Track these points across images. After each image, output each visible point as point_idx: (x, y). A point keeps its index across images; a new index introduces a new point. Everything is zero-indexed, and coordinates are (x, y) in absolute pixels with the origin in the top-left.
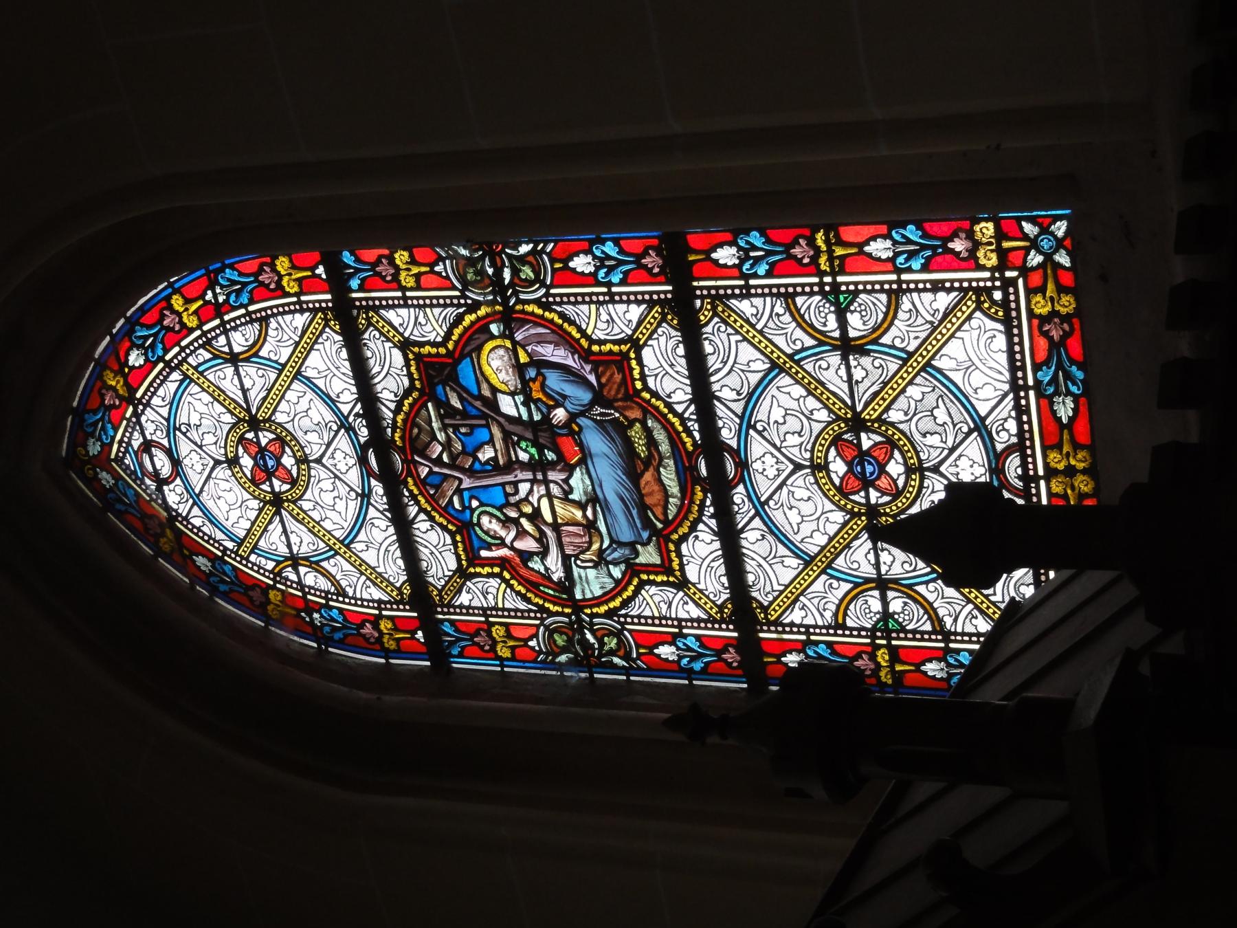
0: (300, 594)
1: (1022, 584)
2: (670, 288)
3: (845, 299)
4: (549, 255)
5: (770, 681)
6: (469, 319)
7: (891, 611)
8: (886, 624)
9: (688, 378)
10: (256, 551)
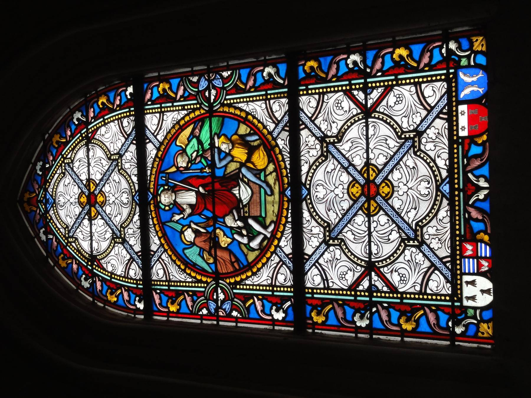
1: (429, 226)
2: (286, 90)
3: (302, 114)
4: (227, 91)
5: (154, 313)
6: (244, 277)
7: (280, 245)
8: (218, 314)
9: (304, 232)
10: (433, 268)
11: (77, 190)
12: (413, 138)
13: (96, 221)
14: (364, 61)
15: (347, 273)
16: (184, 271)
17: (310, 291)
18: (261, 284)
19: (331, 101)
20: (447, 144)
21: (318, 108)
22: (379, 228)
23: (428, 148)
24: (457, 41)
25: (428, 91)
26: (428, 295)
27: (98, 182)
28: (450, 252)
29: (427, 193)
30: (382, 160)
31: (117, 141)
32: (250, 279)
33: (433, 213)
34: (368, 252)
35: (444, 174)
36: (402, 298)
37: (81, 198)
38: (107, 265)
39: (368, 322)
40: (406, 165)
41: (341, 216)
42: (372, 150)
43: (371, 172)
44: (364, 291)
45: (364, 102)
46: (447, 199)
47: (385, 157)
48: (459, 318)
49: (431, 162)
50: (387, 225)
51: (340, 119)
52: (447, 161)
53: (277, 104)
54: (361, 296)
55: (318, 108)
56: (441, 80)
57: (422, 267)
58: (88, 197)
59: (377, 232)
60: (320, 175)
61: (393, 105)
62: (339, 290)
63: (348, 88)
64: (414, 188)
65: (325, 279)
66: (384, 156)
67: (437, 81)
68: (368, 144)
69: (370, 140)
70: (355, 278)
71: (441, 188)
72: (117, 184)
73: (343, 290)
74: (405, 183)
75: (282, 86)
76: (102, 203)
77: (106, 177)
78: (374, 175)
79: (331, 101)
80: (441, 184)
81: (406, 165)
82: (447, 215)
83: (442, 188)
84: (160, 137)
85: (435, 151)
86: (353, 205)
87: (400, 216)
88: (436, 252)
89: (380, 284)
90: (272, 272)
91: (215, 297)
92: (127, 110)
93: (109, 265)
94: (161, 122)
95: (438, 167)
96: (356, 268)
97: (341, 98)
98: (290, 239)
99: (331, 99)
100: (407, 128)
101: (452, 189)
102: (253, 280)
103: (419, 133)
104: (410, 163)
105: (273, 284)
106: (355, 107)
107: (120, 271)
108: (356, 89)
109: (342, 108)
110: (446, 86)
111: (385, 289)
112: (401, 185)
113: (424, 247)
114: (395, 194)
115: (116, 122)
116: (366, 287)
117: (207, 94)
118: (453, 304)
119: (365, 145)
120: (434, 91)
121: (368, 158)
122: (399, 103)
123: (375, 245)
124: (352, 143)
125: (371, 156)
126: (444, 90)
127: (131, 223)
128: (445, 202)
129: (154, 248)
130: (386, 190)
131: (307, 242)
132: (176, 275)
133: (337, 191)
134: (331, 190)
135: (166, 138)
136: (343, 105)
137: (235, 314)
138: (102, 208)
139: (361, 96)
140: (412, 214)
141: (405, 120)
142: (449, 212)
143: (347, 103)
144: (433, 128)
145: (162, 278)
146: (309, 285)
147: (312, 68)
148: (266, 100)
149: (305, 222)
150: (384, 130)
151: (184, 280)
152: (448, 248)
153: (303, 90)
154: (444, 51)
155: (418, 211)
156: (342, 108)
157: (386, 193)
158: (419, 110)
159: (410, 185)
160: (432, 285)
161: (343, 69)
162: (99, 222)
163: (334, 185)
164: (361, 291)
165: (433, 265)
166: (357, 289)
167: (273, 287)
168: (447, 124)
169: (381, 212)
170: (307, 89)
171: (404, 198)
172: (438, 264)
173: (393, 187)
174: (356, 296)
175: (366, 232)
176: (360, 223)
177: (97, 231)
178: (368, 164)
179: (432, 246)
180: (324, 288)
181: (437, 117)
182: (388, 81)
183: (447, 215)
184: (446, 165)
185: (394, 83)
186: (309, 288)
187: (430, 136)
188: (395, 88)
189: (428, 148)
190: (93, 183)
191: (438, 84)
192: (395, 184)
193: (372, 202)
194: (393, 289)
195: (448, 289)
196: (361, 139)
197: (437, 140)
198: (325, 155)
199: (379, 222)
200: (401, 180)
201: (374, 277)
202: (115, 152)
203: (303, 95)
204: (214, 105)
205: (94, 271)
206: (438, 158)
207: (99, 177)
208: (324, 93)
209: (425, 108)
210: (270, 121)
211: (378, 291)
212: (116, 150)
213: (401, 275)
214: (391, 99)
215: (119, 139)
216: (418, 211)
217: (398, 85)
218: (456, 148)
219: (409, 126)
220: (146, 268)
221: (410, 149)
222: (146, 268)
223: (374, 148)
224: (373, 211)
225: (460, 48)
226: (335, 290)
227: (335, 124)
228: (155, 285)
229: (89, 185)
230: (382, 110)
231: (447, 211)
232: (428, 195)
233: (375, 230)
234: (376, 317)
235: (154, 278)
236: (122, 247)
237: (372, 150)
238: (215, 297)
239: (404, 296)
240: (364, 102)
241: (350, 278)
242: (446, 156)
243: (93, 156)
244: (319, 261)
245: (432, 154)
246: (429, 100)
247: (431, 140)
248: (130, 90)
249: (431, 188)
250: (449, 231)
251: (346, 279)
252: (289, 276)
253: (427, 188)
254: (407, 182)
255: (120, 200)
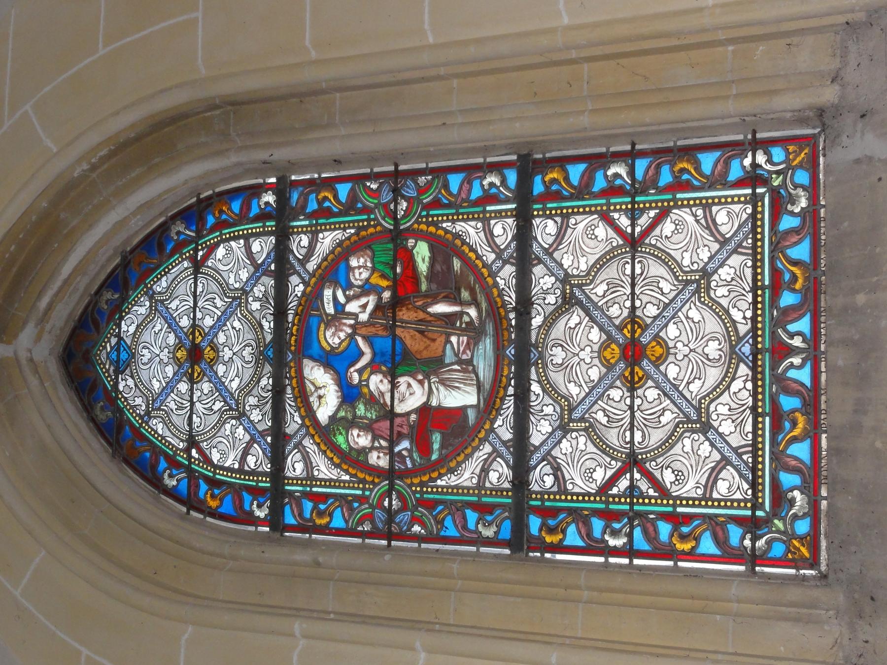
0: (187, 463)
11: (172, 339)
12: (571, 420)
13: (199, 385)
14: (632, 173)
15: (595, 470)
16: (337, 466)
17: (539, 496)
18: (684, 495)
19: (691, 484)
20: (514, 297)
21: (560, 236)
22: (646, 405)
23: (719, 293)
24: (767, 153)
25: (256, 247)
26: (713, 500)
27: (207, 330)
28: (270, 424)
29: (718, 357)
30: (652, 311)
31: (566, 253)
32: (445, 478)
33: (723, 386)
34: (628, 439)
35: (743, 329)
36: (674, 506)
37: (177, 351)
38: (662, 470)
39: (625, 540)
40: (687, 318)
41: (164, 385)
42: (638, 296)
43: (197, 334)
44: (620, 497)
45: (629, 230)
46: (114, 366)
47: (656, 307)
48: (760, 532)
49: (722, 314)
50: (656, 402)
51: (595, 251)
52: (272, 323)
53: (499, 226)
54: (614, 503)
55: (560, 236)
56: (739, 202)
57: (243, 441)
58: (190, 352)
59: (625, 294)
60: (558, 331)
61: (598, 468)
62: (583, 495)
63: (629, 206)
64: (699, 350)
65: (248, 248)
66: (654, 305)
67: (733, 202)
68: (633, 285)
69: (636, 280)
70: (607, 477)
71: (737, 350)
72: (697, 325)
73: (589, 494)
74: (686, 343)
75: (507, 201)
76: (658, 359)
77: (220, 323)
78: (200, 338)
79: (581, 226)
80: (737, 344)
81: (687, 318)
82: (745, 387)
83: (740, 350)
84: (311, 266)
85: (542, 403)
86: (606, 374)
87: (677, 389)
88: (726, 438)
89: (644, 485)
90: (706, 475)
91: (386, 503)
92: (365, 217)
93: (214, 451)
94: (485, 471)
95: (734, 322)
96: (610, 464)
97: (595, 222)
98: (291, 294)
99: (581, 224)
100: (689, 266)
101: (755, 352)
102: (449, 479)
103: (706, 274)
104: (694, 314)
105: (708, 496)
106: (615, 236)
107: (690, 488)
108: (615, 210)
109: (673, 472)
110: (274, 241)
111: (651, 492)
112: (679, 345)
113: (559, 433)
114: (671, 358)
115: (242, 241)
116: (622, 489)
117: (392, 206)
118: (754, 513)
119: (192, 302)
120: (262, 247)
121: (633, 308)
122: (678, 232)
123: (638, 429)
124: (660, 422)
125: (638, 303)
126: (745, 216)
127: (727, 392)
128: (744, 370)
129: (509, 270)
130: (659, 350)
131: (738, 273)
132: (324, 469)
133: (582, 355)
134: (695, 352)
135: (319, 267)
136: (672, 478)
137: (417, 528)
138: (657, 367)
139: (624, 222)
140: (695, 387)
141: (581, 446)
142: (271, 380)
143: (602, 231)
144: (726, 267)
145: (550, 488)
146: (535, 487)
147: (492, 185)
148: (486, 221)
149: (271, 318)
150: (656, 269)
151: (336, 478)
152: (747, 436)
153: (538, 210)
154: (747, 162)
155: (704, 382)
156: (596, 237)
157: (657, 355)
158: (563, 457)
159: (692, 346)
160: (722, 487)
161: (255, 211)
162: (206, 387)
163: (690, 360)
164: (614, 496)
165: (724, 458)
166: (610, 492)
167: (632, 496)
168: (273, 282)
169: (617, 322)
170: (544, 209)
171: (684, 364)
172: (734, 458)
173: (668, 348)
174: (607, 503)
175: (626, 412)
176: (617, 399)
177: (642, 408)
178: (194, 326)
179: (721, 430)
180: (559, 492)
181: (735, 251)
182: (663, 201)
183: (745, 387)
184: (745, 318)
185: (672, 204)
186: (537, 493)
187: (723, 278)
188: (674, 211)
189: (719, 293)
190: (199, 331)
191: (736, 208)
192: (671, 344)
193: (637, 369)
194: (663, 491)
195: (746, 494)
196: (188, 296)
197: (539, 418)
198: (568, 302)
199: (646, 397)
200: (679, 339)
201: (637, 476)
202: (237, 285)
203: (538, 216)
204: (402, 222)
205: (193, 466)
206: (539, 394)
207: (208, 322)
208: (704, 498)
209: (717, 240)
210: (489, 249)
211: (642, 495)
212: (696, 265)
213: (593, 237)
214: (668, 227)
215: (566, 454)
216: (704, 382)
217: (676, 206)
218: (760, 296)
219: (692, 265)
220: (278, 458)
221: (694, 294)
222: (278, 458)
223: (641, 293)
224: (638, 382)
225: (770, 161)
226: (578, 495)
227: (585, 259)
228: (288, 484)
229: (193, 333)
230: (653, 242)
231: (269, 378)
232: (553, 346)
233: (638, 409)
234: (638, 533)
235: (289, 474)
236: (238, 423)
237: (638, 296)
238: (386, 503)
239: (546, 497)
240: (629, 230)
241: (600, 476)
242: (744, 305)
243: (203, 292)
244: (553, 453)
245: (724, 302)
246: (723, 229)
247: (725, 283)
248: (269, 198)
249: (256, 354)
250: (512, 406)
251: (593, 480)
252: (507, 472)
253: (143, 356)
254: (689, 342)
255: (702, 353)
